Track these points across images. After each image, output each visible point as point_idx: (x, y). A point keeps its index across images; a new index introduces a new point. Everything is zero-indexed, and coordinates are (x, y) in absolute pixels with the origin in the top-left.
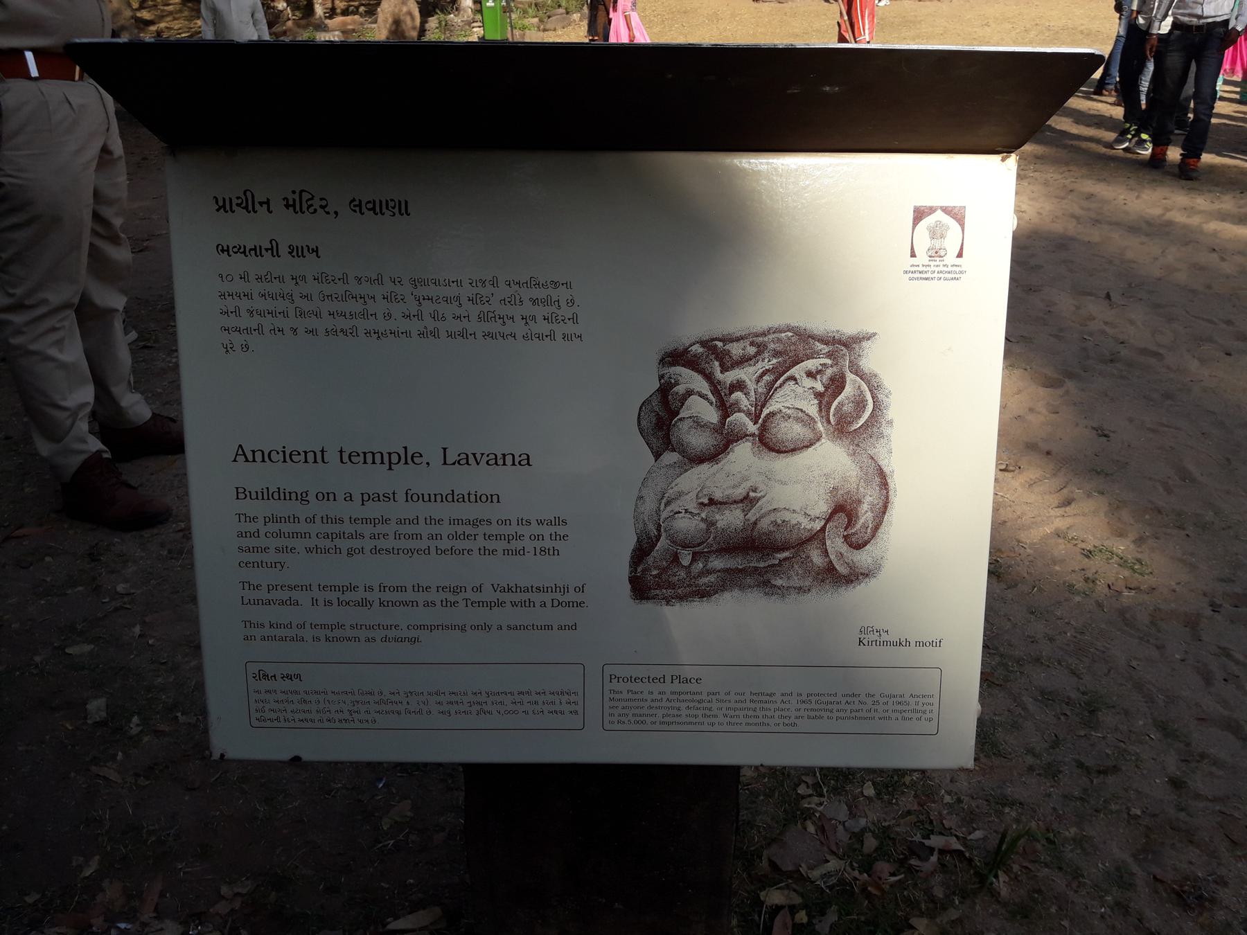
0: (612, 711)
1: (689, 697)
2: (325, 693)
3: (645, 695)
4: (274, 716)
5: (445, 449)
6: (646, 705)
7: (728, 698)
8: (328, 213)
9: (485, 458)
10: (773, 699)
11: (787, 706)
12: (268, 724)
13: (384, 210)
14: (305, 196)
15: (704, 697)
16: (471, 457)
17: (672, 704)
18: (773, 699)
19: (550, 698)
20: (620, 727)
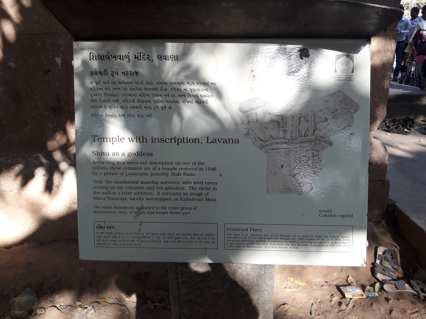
0: (228, 242)
1: (257, 237)
2: (122, 234)
3: (241, 236)
4: (103, 242)
5: (208, 137)
6: (241, 239)
7: (272, 237)
8: (150, 60)
9: (222, 141)
10: (289, 238)
11: (294, 241)
12: (101, 246)
13: (169, 59)
14: (142, 54)
15: (263, 236)
16: (217, 140)
17: (251, 239)
18: (289, 238)
19: (205, 237)
20: (231, 248)
